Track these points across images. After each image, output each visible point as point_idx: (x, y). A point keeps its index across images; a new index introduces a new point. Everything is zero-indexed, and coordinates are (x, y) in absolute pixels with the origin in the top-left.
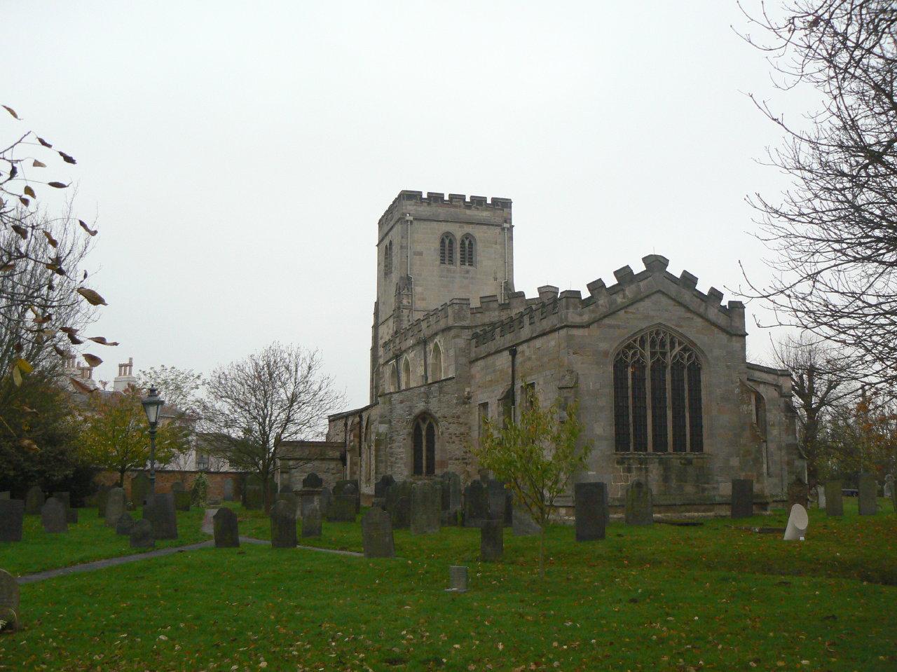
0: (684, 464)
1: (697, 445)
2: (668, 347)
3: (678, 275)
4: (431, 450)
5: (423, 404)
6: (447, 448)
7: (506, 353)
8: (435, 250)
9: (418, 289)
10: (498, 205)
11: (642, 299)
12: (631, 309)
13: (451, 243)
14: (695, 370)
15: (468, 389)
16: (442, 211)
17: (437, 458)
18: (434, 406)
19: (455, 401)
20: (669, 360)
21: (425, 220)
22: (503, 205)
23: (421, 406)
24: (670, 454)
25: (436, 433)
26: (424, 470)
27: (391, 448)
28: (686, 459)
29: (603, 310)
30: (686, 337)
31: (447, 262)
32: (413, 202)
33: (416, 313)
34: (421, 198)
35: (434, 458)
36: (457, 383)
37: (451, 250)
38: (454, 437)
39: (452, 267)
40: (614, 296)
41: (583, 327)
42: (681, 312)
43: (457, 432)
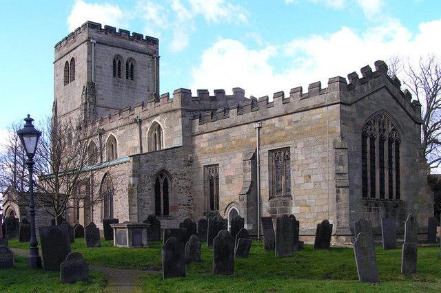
4: (166, 198)
6: (177, 196)
9: (100, 92)
12: (371, 97)
13: (120, 63)
15: (190, 155)
17: (171, 204)
20: (386, 135)
21: (104, 44)
23: (160, 166)
25: (170, 186)
26: (162, 213)
42: (394, 103)
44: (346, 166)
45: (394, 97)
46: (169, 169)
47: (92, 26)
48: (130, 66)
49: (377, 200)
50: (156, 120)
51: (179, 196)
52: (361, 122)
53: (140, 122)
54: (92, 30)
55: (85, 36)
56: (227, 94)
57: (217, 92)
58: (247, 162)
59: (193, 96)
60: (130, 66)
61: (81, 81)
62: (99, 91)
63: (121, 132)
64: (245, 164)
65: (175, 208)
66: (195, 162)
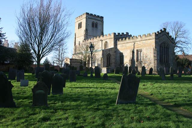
1: (168, 61)
9: (88, 31)
14: (168, 49)
22: (102, 18)
23: (108, 53)
29: (159, 36)
47: (87, 14)
52: (160, 43)
65: (112, 64)
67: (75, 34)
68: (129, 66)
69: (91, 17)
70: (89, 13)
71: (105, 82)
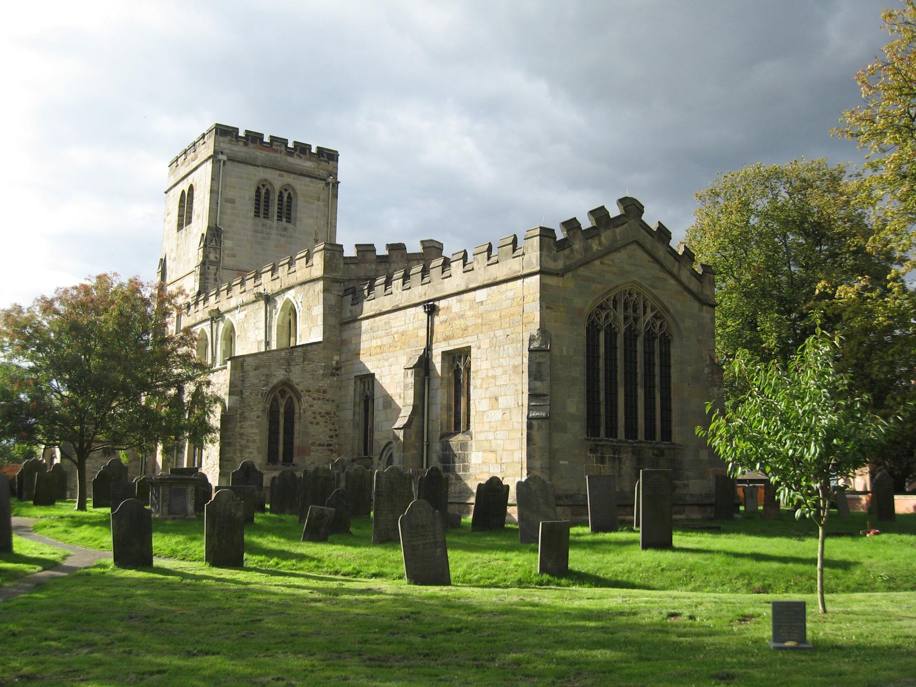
0: (657, 455)
1: (667, 434)
2: (640, 311)
3: (654, 226)
5: (283, 372)
6: (311, 429)
7: (420, 311)
8: (250, 199)
9: (227, 244)
10: (323, 156)
11: (617, 250)
12: (606, 260)
13: (268, 193)
14: (666, 342)
15: (336, 358)
16: (261, 155)
17: (297, 442)
18: (296, 376)
19: (321, 372)
20: (641, 326)
22: (329, 156)
23: (279, 375)
24: (641, 442)
25: (297, 411)
26: (281, 458)
27: (241, 427)
28: (658, 449)
29: (578, 256)
30: (661, 303)
31: (262, 215)
32: (227, 139)
33: (225, 271)
34: (237, 137)
35: (292, 443)
36: (324, 348)
37: (267, 206)
38: (318, 417)
39: (268, 222)
40: (590, 241)
41: (557, 275)
42: (655, 270)
43: (323, 411)
44: (547, 382)
45: (656, 260)
46: (297, 381)
47: (222, 131)
48: (285, 198)
49: (620, 441)
50: (290, 295)
51: (313, 429)
52: (585, 304)
53: (269, 299)
54: (222, 139)
55: (207, 150)
56: (409, 250)
57: (392, 247)
58: (410, 371)
59: (612, 215)
60: (285, 198)
61: (200, 223)
62: (226, 241)
63: (242, 314)
64: (406, 376)
65: (305, 451)
66: (343, 370)
67: (163, 263)
68: (514, 475)
69: (252, 151)
70: (236, 130)
71: (567, 614)
